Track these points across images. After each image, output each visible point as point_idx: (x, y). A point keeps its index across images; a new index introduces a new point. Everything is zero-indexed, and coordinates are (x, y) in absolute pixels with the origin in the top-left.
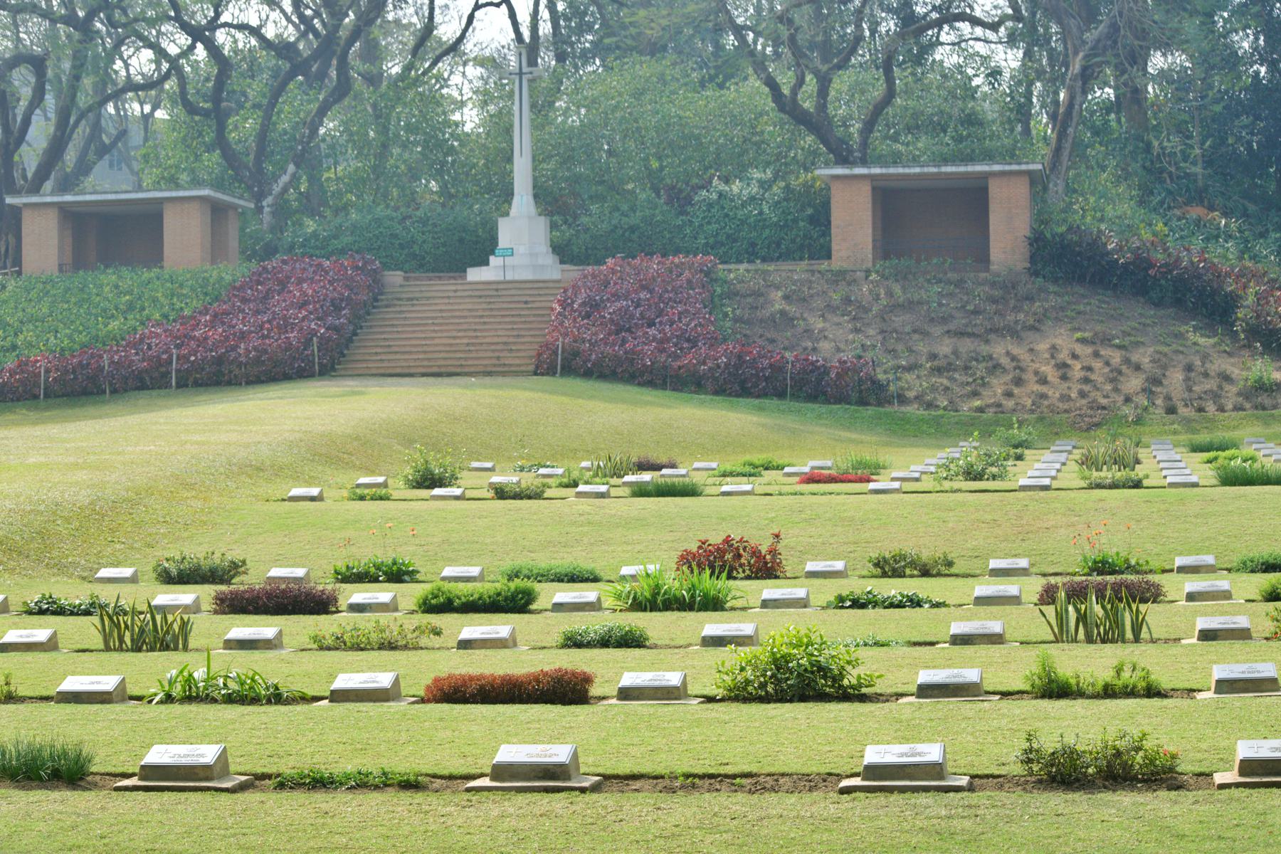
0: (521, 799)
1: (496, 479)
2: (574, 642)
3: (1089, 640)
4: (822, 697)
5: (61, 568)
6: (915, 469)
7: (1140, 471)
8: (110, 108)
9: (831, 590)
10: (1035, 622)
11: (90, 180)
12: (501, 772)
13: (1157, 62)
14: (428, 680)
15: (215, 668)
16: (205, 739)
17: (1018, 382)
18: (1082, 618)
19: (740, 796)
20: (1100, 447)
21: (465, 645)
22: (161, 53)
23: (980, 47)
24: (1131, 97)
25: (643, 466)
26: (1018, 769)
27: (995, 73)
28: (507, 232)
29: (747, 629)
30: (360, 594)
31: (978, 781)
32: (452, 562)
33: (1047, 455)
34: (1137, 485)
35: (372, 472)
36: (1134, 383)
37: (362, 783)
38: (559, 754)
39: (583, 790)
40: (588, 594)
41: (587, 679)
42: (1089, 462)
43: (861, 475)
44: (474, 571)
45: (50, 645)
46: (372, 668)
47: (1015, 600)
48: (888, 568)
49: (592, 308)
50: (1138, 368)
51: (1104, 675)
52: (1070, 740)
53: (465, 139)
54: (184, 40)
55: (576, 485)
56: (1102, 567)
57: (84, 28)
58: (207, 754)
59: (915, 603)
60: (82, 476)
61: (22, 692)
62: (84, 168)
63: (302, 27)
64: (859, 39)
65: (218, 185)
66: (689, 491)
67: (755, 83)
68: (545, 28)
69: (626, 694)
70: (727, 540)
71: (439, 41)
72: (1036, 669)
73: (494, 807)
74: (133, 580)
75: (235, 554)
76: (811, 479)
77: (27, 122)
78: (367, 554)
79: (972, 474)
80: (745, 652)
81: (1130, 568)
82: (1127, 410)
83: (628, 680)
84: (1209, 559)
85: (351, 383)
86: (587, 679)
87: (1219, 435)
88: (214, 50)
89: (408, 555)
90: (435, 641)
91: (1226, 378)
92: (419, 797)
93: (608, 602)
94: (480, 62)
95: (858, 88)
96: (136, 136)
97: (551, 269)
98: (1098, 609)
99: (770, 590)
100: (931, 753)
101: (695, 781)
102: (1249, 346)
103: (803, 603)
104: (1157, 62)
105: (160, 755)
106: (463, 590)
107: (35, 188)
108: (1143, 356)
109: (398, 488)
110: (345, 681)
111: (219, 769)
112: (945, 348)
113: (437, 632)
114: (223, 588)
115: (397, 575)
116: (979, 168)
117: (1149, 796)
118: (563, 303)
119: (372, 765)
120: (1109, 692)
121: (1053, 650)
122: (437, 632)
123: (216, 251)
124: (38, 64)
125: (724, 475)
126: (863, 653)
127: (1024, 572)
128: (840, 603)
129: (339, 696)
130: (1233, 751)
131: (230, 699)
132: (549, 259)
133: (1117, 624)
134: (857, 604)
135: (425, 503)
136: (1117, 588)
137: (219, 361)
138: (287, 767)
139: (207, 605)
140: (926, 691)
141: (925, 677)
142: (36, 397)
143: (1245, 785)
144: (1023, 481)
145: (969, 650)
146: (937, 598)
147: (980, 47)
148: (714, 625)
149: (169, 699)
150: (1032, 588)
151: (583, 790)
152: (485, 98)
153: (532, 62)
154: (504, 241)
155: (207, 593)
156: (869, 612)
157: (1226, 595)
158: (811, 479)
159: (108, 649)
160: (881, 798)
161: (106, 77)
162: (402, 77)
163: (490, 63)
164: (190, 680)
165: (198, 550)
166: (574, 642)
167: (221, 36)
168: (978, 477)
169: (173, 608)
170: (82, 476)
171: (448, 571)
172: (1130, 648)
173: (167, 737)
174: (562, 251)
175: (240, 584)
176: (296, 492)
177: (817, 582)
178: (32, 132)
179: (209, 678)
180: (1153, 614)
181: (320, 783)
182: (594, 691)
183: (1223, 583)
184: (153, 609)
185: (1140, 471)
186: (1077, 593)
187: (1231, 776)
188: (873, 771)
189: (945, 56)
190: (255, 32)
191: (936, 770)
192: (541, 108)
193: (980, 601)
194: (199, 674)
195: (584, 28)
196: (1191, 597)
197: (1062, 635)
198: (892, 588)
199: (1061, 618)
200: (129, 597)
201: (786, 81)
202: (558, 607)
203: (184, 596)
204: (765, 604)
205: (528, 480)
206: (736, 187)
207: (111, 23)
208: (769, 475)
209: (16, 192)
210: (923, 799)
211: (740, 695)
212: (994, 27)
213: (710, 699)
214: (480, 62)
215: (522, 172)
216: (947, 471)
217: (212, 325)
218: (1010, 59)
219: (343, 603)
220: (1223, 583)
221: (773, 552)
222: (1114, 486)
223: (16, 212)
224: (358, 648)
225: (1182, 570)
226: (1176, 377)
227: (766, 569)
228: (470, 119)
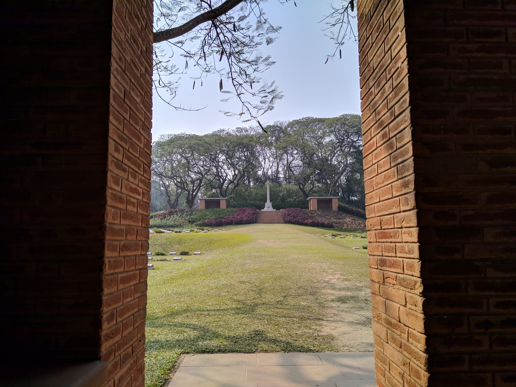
49: (289, 214)
174: (274, 207)
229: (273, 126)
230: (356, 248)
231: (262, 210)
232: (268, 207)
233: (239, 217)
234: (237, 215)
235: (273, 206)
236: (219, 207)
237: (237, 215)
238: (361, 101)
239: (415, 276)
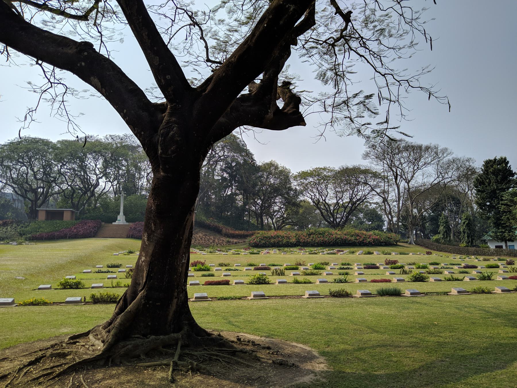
4: (262, 284)
17: (196, 240)
41: (229, 281)
47: (251, 270)
49: (135, 228)
79: (210, 252)
86: (229, 281)
91: (223, 240)
102: (224, 237)
107: (40, 207)
118: (130, 228)
120: (305, 283)
123: (72, 218)
132: (125, 222)
137: (76, 234)
142: (43, 239)
143: (254, 299)
154: (118, 219)
168: (212, 253)
174: (127, 220)
182: (230, 283)
187: (194, 299)
211: (251, 283)
217: (74, 229)
229: (34, 138)
230: (237, 265)
231: (113, 223)
232: (121, 219)
233: (75, 230)
234: (75, 228)
235: (126, 220)
236: (62, 219)
237: (75, 228)
238: (212, 73)
239: (270, 297)
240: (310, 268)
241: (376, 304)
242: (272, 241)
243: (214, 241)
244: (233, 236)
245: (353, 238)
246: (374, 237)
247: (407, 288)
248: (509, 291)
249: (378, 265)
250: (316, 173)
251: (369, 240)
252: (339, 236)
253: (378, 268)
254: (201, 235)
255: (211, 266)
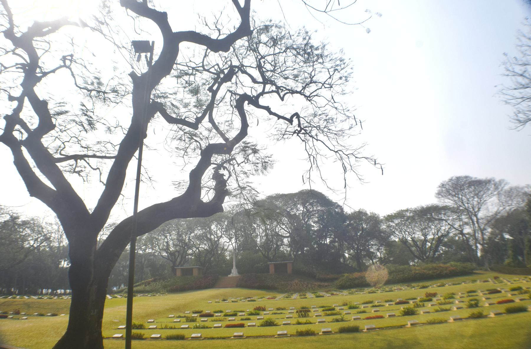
0: (237, 340)
1: (232, 300)
2: (242, 320)
3: (302, 317)
5: (181, 312)
6: (280, 297)
7: (306, 296)
8: (187, 257)
9: (272, 312)
10: (296, 315)
11: (184, 265)
12: (235, 336)
13: (305, 249)
14: (225, 325)
15: (200, 324)
16: (199, 333)
18: (302, 315)
19: (263, 339)
20: (301, 294)
21: (229, 320)
22: (193, 251)
23: (285, 248)
24: (302, 252)
25: (249, 298)
26: (295, 334)
27: (287, 251)
28: (232, 271)
29: (262, 317)
30: (216, 314)
31: (291, 336)
32: (227, 310)
33: (295, 295)
34: (306, 298)
35: (217, 299)
36: (305, 286)
37: (218, 338)
38: (241, 334)
39: (244, 338)
40: (243, 314)
42: (300, 295)
43: (274, 298)
44: (230, 311)
45: (180, 321)
46: (218, 324)
47: (293, 313)
48: (278, 309)
50: (305, 284)
51: (305, 321)
52: (302, 330)
53: (228, 260)
54: (195, 249)
55: (241, 300)
56: (303, 308)
57: (184, 247)
58: (199, 335)
59: (282, 313)
60: (183, 300)
61: (176, 327)
62: (184, 264)
63: (68, 291)
64: (272, 247)
65: (199, 266)
66: (254, 301)
67: (260, 253)
68: (237, 247)
69: (249, 326)
70: (259, 307)
71: (225, 249)
72: (297, 321)
73: (233, 341)
74: (190, 313)
75: (202, 310)
76: (268, 299)
77: (177, 258)
78: (217, 309)
79: (287, 297)
80: (262, 320)
81: (307, 308)
82: (304, 289)
83: (249, 324)
84: (315, 306)
85: (217, 289)
87: (316, 291)
88: (199, 250)
89: (222, 309)
90: (226, 320)
91: (315, 284)
92: (225, 340)
93: (246, 314)
94: (229, 251)
95: (272, 253)
96: (190, 260)
97: (237, 275)
98: (303, 313)
99: (265, 312)
100: (285, 332)
101: (257, 337)
103: (268, 314)
104: (305, 249)
105: (193, 335)
106: (229, 313)
107: (178, 266)
108: (306, 283)
109: (221, 301)
110: (215, 325)
111: (201, 337)
112: (283, 283)
113: (226, 319)
114: (200, 314)
115: (221, 312)
116: (286, 262)
117: (312, 337)
119: (219, 336)
120: (306, 323)
121: (298, 319)
122: (226, 319)
124: (179, 252)
125: (259, 298)
126: (276, 320)
127: (294, 309)
128: (273, 314)
129: (215, 327)
130: (321, 330)
131: (202, 328)
132: (237, 274)
133: (306, 315)
134: (275, 314)
135: (224, 303)
136: (305, 310)
138: (209, 336)
139: (198, 316)
140: (284, 324)
141: (284, 323)
144: (293, 298)
145: (288, 319)
146: (284, 313)
147: (285, 248)
148: (258, 317)
149: (194, 328)
150: (295, 311)
151: (244, 338)
152: (230, 255)
153: (235, 251)
155: (198, 314)
156: (276, 315)
157: (318, 311)
158: (268, 299)
159: (187, 322)
160: (280, 338)
161: (187, 253)
162: (220, 253)
163: (230, 251)
164: (197, 326)
165: (197, 309)
166: (242, 320)
167: (200, 249)
169: (195, 317)
170: (183, 300)
171: (227, 311)
172: (307, 318)
173: (194, 333)
174: (239, 273)
175: (202, 313)
176: (209, 302)
177: (270, 311)
178: (178, 259)
179: (199, 325)
180: (309, 313)
181: (213, 338)
182: (245, 326)
183: (317, 309)
184: (192, 317)
185: (306, 296)
186: (301, 311)
188: (279, 335)
189: (281, 249)
190: (204, 248)
191: (286, 334)
192: (236, 257)
193: (289, 313)
194: (198, 325)
195: (241, 247)
196: (314, 311)
197: (299, 317)
198: (279, 312)
199: (299, 314)
200: (189, 315)
201: (264, 253)
202: (240, 315)
203: (196, 315)
204: (264, 314)
205: (236, 300)
206: (258, 265)
207: (187, 247)
208: (263, 298)
209: (176, 267)
210: (285, 338)
211: (262, 326)
212: (287, 246)
213: (258, 326)
214: (229, 251)
215: (234, 263)
216: (284, 297)
218: (289, 249)
219: (215, 316)
220: (317, 309)
221: (265, 308)
222: (304, 298)
223: (176, 269)
224: (216, 321)
225: (313, 308)
226: (310, 286)
227: (264, 310)
228: (228, 258)
231: (229, 276)
232: (234, 272)
240: (442, 298)
241: (316, 341)
242: (356, 282)
243: (307, 286)
244: (325, 280)
245: (430, 272)
246: (452, 268)
247: (365, 325)
248: (461, 319)
249: (499, 289)
250: (400, 215)
251: (445, 272)
252: (417, 272)
253: (499, 292)
254: (297, 281)
255: (356, 304)
